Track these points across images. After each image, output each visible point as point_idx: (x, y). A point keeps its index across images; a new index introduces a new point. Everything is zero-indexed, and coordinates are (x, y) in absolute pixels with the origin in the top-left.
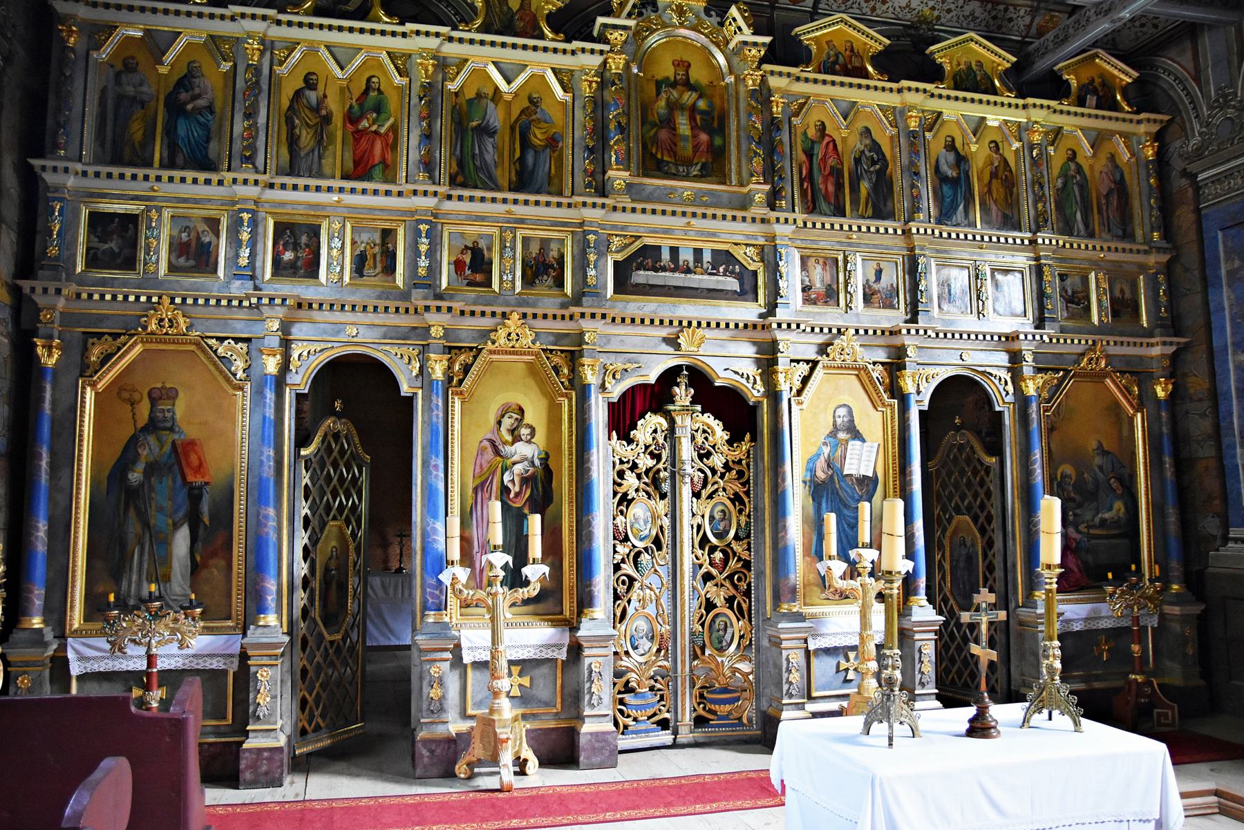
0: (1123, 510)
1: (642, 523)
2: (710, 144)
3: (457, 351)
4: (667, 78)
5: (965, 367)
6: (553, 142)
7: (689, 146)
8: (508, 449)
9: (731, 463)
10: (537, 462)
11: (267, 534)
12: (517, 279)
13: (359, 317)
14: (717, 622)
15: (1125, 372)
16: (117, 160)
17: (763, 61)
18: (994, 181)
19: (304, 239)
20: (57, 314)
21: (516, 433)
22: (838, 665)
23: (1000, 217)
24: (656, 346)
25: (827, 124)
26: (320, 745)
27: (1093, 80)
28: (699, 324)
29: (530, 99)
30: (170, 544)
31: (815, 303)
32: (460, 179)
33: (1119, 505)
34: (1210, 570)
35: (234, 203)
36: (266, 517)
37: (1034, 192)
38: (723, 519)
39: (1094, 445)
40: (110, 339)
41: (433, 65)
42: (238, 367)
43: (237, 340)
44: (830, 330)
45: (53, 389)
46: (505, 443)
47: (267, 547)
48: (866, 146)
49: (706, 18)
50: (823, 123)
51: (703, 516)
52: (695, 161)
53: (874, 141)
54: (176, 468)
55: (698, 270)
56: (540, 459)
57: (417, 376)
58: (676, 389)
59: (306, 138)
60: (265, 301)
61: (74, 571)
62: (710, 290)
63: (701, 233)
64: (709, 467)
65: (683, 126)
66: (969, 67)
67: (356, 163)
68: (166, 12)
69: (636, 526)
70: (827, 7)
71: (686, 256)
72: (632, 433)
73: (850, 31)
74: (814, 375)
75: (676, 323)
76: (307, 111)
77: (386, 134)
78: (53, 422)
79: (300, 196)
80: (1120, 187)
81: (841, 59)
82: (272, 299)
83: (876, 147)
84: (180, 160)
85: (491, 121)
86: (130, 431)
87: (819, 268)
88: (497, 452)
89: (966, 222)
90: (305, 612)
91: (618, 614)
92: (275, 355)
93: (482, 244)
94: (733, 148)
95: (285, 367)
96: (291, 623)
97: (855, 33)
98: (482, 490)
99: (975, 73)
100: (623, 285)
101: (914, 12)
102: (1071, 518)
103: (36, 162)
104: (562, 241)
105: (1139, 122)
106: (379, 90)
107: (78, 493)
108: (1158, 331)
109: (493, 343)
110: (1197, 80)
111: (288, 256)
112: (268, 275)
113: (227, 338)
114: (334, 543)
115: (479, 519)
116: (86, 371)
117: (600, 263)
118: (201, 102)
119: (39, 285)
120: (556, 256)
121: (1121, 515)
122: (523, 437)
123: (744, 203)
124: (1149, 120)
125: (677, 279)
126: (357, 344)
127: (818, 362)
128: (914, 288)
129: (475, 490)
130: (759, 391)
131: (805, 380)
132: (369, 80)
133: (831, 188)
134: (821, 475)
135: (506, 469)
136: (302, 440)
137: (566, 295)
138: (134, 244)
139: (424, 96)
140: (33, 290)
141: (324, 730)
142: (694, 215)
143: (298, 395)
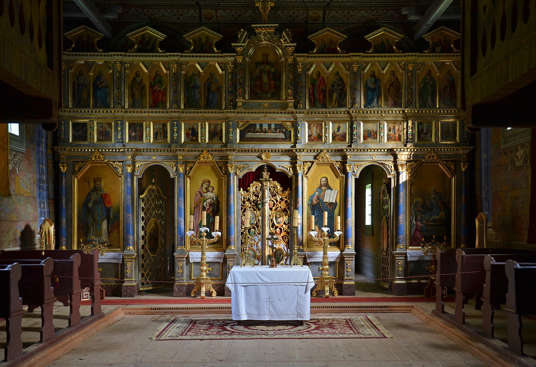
0: (444, 215)
3: (188, 163)
4: (260, 61)
5: (374, 161)
6: (219, 90)
10: (215, 199)
11: (129, 222)
12: (206, 138)
13: (156, 153)
14: (277, 252)
17: (293, 53)
18: (391, 88)
19: (138, 128)
20: (65, 156)
21: (208, 189)
25: (321, 72)
26: (148, 288)
28: (268, 151)
29: (211, 74)
30: (101, 225)
31: (313, 141)
32: (187, 105)
33: (442, 214)
35: (116, 118)
36: (129, 217)
37: (408, 91)
39: (432, 190)
40: (81, 163)
41: (176, 66)
42: (120, 170)
43: (119, 162)
44: (317, 151)
46: (204, 192)
47: (129, 226)
48: (336, 79)
49: (274, 36)
53: (340, 77)
54: (102, 202)
55: (270, 131)
56: (216, 198)
59: (137, 94)
60: (126, 150)
61: (74, 233)
63: (269, 118)
64: (275, 200)
65: (265, 79)
66: (382, 42)
67: (154, 102)
70: (329, 21)
71: (265, 127)
72: (248, 188)
73: (331, 34)
75: (260, 151)
76: (137, 85)
78: (66, 189)
79: (136, 114)
81: (327, 47)
82: (128, 149)
83: (341, 79)
84: (98, 104)
85: (197, 84)
86: (88, 191)
87: (315, 128)
88: (201, 196)
89: (377, 106)
90: (143, 247)
92: (130, 167)
93: (195, 127)
95: (134, 170)
96: (138, 250)
97: (333, 35)
98: (197, 208)
99: (384, 44)
101: (365, 18)
104: (222, 124)
106: (160, 75)
107: (74, 210)
109: (199, 160)
111: (133, 134)
112: (127, 140)
113: (116, 161)
114: (153, 225)
115: (196, 217)
116: (74, 173)
118: (104, 84)
123: (285, 107)
125: (262, 135)
126: (156, 162)
127: (314, 162)
128: (351, 134)
129: (195, 208)
130: (291, 173)
131: (309, 169)
132: (156, 72)
133: (321, 97)
134: (315, 202)
135: (205, 201)
136: (141, 192)
137: (223, 142)
138: (86, 133)
139: (174, 77)
140: (58, 149)
141: (150, 284)
142: (267, 113)
143: (139, 179)
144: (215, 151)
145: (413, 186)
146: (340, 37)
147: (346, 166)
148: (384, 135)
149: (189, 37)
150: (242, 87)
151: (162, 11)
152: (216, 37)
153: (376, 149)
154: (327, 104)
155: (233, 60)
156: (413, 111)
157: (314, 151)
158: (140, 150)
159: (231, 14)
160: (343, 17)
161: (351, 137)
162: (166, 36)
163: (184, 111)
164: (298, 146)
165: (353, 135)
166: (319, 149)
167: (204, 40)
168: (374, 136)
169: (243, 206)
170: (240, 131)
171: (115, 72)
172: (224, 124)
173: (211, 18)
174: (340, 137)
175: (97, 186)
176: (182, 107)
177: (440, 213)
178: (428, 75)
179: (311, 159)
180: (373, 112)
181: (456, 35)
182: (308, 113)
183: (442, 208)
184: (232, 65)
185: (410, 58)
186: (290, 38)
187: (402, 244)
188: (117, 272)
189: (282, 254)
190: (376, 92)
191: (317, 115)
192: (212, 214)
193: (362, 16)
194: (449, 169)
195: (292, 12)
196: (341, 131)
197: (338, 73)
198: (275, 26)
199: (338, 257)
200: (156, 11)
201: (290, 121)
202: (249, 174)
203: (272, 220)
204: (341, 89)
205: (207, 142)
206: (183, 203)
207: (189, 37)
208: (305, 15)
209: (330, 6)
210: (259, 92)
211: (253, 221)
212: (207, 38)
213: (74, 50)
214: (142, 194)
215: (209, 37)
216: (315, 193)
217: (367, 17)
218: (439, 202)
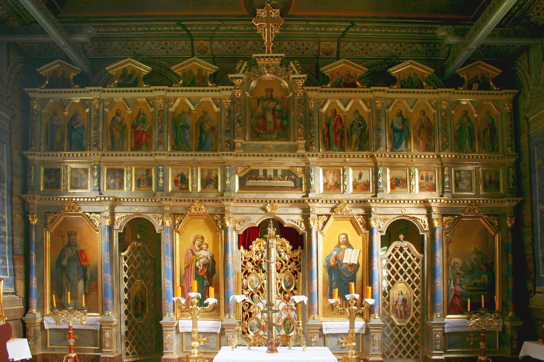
1: (254, 282)
2: (281, 124)
3: (177, 215)
4: (263, 97)
5: (404, 216)
7: (272, 126)
8: (197, 253)
9: (293, 258)
10: (209, 258)
14: (287, 322)
15: (491, 215)
16: (52, 149)
21: (201, 247)
22: (338, 341)
23: (424, 146)
24: (257, 211)
25: (337, 110)
28: (274, 201)
31: (329, 190)
32: (176, 147)
34: (530, 306)
38: (290, 281)
39: (473, 249)
40: (54, 214)
43: (96, 213)
44: (335, 201)
45: (36, 232)
46: (196, 251)
48: (356, 118)
50: (335, 110)
51: (281, 280)
52: (274, 132)
55: (275, 178)
56: (211, 257)
57: (161, 225)
58: (269, 229)
59: (117, 135)
60: (103, 199)
62: (266, 187)
64: (283, 260)
65: (269, 117)
66: (410, 77)
67: (136, 144)
68: (65, 92)
69: (252, 283)
70: (343, 55)
71: (270, 173)
74: (329, 221)
75: (264, 201)
76: (117, 125)
77: (147, 132)
80: (492, 128)
83: (361, 118)
84: (73, 148)
87: (331, 175)
88: (194, 254)
91: (244, 318)
93: (185, 173)
94: (292, 124)
98: (188, 269)
99: (412, 79)
102: (458, 282)
103: (25, 152)
104: (217, 170)
105: (501, 94)
108: (507, 195)
110: (528, 72)
111: (112, 181)
114: (139, 288)
117: (232, 178)
118: (79, 125)
119: (28, 196)
120: (215, 176)
121: (486, 281)
122: (204, 248)
123: (294, 149)
124: (506, 93)
128: (376, 183)
129: (185, 268)
130: (303, 229)
131: (325, 223)
132: (140, 110)
133: (338, 139)
134: (332, 263)
136: (122, 249)
137: (219, 192)
138: (59, 179)
144: (209, 201)
145: (451, 244)
146: (360, 70)
147: (370, 221)
148: (415, 184)
149: (178, 69)
150: (241, 126)
151: (149, 43)
152: (209, 68)
153: (406, 200)
154: (346, 147)
155: (230, 94)
156: (450, 156)
157: (331, 201)
158: (120, 200)
159: (228, 46)
161: (375, 185)
162: (150, 68)
163: (170, 153)
164: (311, 195)
165: (379, 183)
166: (337, 200)
167: (195, 73)
168: (403, 185)
169: (244, 267)
170: (240, 178)
171: (92, 110)
172: (219, 170)
173: (206, 52)
174: (362, 186)
175: (72, 241)
176: (169, 149)
177: (483, 276)
178: (463, 116)
179: (328, 211)
180: (399, 158)
181: (495, 72)
182: (323, 156)
183: (484, 270)
184: (229, 100)
185: (443, 96)
186: (299, 70)
187: (440, 312)
188: (95, 339)
189: (293, 324)
190: (404, 133)
191: (333, 159)
192: (207, 276)
193: (383, 50)
195: (300, 43)
196: (364, 179)
197: (357, 111)
198: (281, 57)
199: (362, 328)
200: (141, 44)
201: (300, 167)
202: (253, 229)
203: (279, 284)
204: (362, 130)
205: (198, 191)
206: (170, 263)
207: (178, 69)
208: (316, 47)
209: (346, 36)
210: (261, 132)
211: (257, 286)
212: (200, 70)
213: (48, 87)
214: (124, 251)
215: (202, 69)
216: (332, 252)
217: (388, 52)
218: (481, 263)
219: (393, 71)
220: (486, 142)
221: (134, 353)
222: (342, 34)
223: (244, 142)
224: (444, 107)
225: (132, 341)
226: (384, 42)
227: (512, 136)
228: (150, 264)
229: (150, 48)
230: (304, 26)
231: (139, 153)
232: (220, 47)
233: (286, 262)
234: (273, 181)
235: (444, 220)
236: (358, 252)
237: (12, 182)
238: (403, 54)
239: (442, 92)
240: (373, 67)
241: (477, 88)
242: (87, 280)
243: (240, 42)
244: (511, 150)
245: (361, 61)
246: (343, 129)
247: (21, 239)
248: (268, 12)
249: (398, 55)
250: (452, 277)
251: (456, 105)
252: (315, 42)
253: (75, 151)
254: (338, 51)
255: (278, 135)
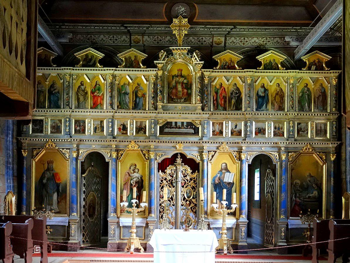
2: (187, 93)
4: (176, 75)
6: (144, 95)
8: (132, 175)
9: (192, 178)
10: (140, 178)
27: (315, 61)
31: (216, 135)
32: (120, 107)
43: (67, 149)
45: (26, 161)
46: (132, 173)
48: (234, 89)
51: (184, 192)
52: (183, 98)
56: (140, 177)
59: (81, 98)
64: (186, 179)
65: (180, 88)
66: (270, 62)
76: (81, 91)
77: (101, 96)
80: (324, 95)
83: (238, 89)
84: (52, 106)
87: (218, 125)
88: (129, 175)
91: (160, 216)
99: (272, 63)
100: (162, 132)
105: (330, 73)
113: (321, 152)
114: (92, 197)
118: (56, 91)
119: (22, 138)
124: (333, 72)
129: (124, 185)
131: (213, 156)
132: (96, 82)
133: (223, 102)
134: (217, 182)
145: (294, 170)
151: (102, 36)
152: (143, 56)
159: (154, 39)
160: (240, 42)
162: (104, 55)
167: (133, 59)
168: (263, 132)
171: (65, 82)
173: (139, 42)
175: (50, 167)
177: (314, 192)
178: (305, 87)
180: (261, 115)
181: (327, 58)
186: (199, 57)
194: (321, 158)
197: (235, 84)
204: (238, 96)
208: (211, 40)
210: (174, 98)
218: (313, 183)
219: (259, 58)
220: (319, 104)
221: (87, 241)
222: (228, 32)
223: (163, 104)
224: (292, 82)
225: (86, 233)
226: (255, 37)
227: (336, 101)
228: (99, 182)
229: (102, 39)
230: (203, 28)
231: (97, 110)
232: (148, 39)
233: (187, 180)
234: (181, 129)
235: (289, 154)
236: (234, 175)
237: (13, 128)
238: (268, 44)
239: (291, 72)
240: (248, 53)
241: (314, 69)
242: (60, 193)
243: (162, 37)
244: (336, 110)
245: (241, 49)
246: (226, 96)
247: (16, 166)
248: (180, 20)
249: (265, 45)
250: (294, 192)
251: (300, 80)
252: (210, 38)
253: (53, 108)
254: (225, 43)
255: (184, 99)
